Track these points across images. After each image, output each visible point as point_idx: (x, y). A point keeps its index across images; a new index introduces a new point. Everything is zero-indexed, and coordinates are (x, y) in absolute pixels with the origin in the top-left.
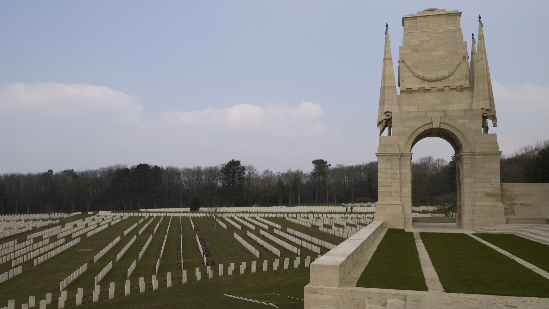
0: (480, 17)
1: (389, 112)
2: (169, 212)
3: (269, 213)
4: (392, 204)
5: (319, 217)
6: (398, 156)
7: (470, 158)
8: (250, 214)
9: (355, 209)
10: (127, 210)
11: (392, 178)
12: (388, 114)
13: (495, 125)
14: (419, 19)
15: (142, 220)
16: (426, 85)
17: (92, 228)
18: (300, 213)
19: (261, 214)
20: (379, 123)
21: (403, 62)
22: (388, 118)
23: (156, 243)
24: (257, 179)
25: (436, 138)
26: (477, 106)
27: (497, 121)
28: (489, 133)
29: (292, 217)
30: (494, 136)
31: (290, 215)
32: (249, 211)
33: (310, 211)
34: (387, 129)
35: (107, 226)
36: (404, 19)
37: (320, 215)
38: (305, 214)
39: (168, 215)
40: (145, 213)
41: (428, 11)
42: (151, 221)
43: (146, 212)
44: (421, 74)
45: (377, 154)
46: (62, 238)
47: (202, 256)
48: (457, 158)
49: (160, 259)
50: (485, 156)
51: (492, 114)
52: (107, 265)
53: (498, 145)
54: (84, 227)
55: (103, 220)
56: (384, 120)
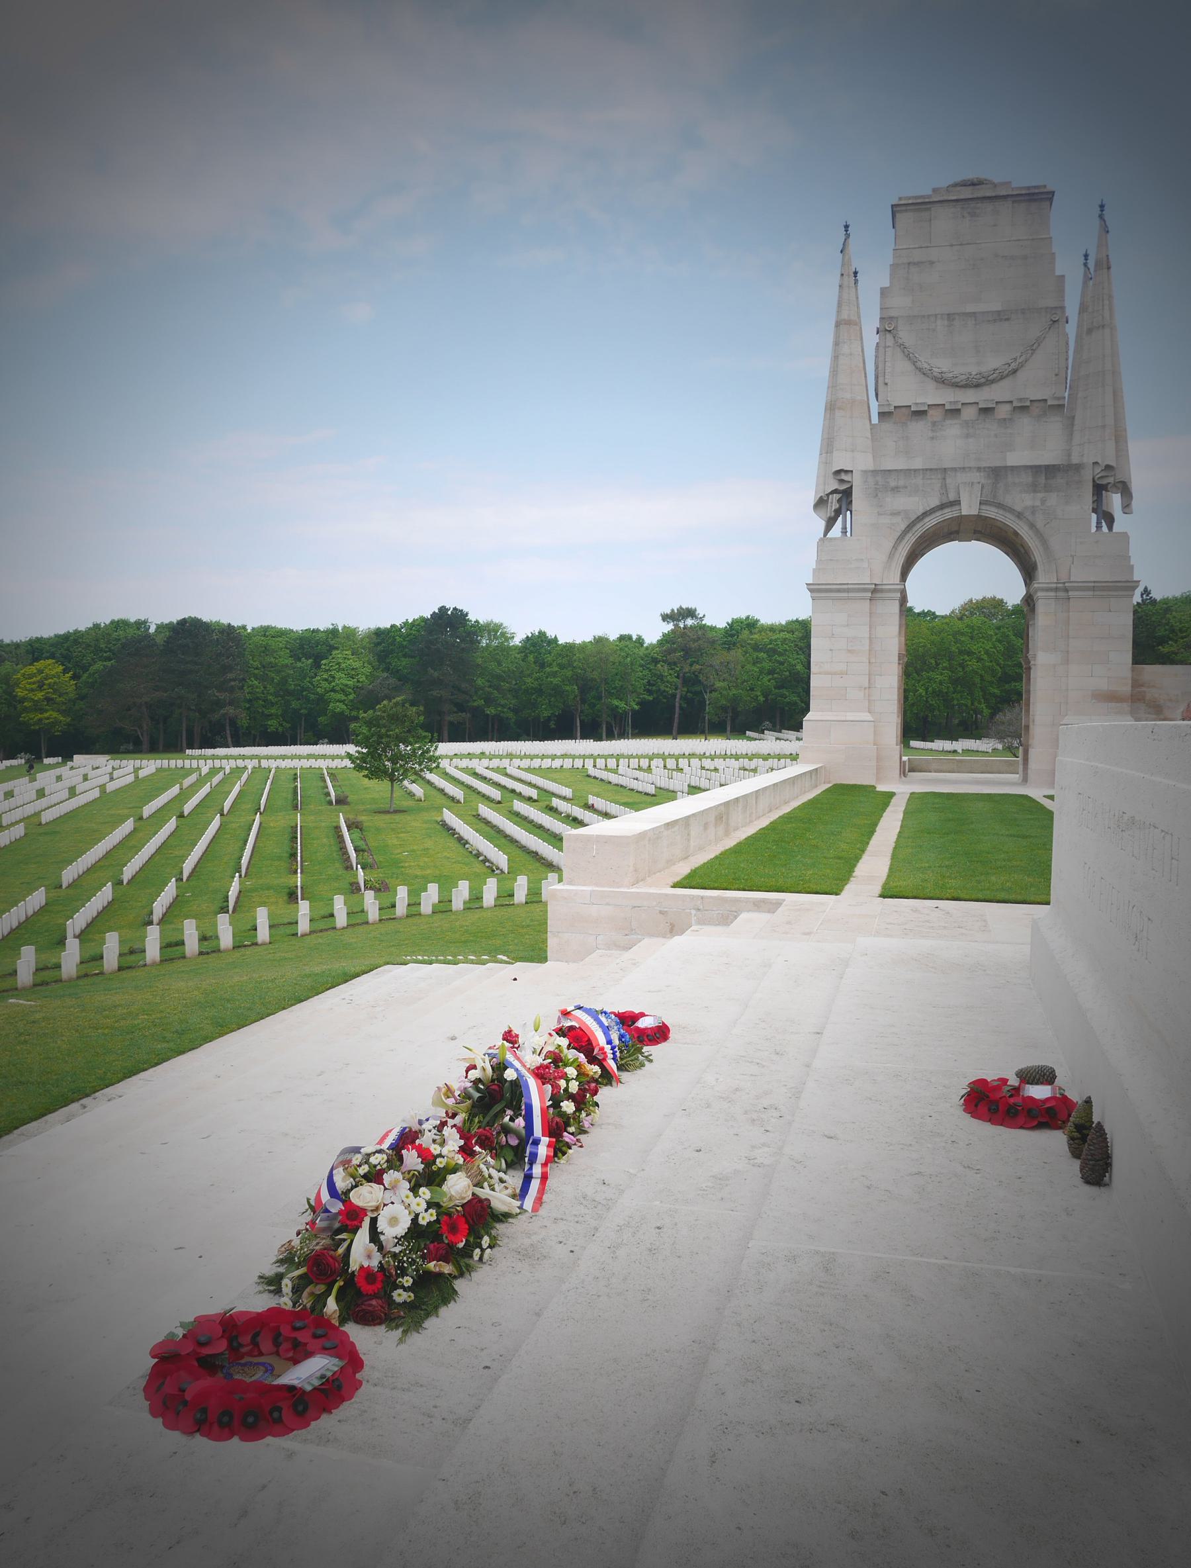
1: (846, 472)
2: (268, 758)
3: (543, 757)
4: (848, 718)
5: (680, 766)
6: (865, 590)
7: (1056, 598)
8: (490, 760)
11: (849, 651)
12: (844, 477)
13: (1126, 511)
15: (192, 778)
17: (54, 799)
18: (630, 757)
19: (532, 760)
20: (820, 503)
21: (890, 331)
22: (844, 487)
23: (231, 835)
26: (1082, 456)
27: (1132, 497)
28: (1114, 531)
29: (606, 768)
30: (1125, 536)
31: (600, 763)
32: (487, 753)
33: (656, 752)
35: (96, 794)
36: (895, 209)
37: (683, 763)
38: (642, 760)
39: (264, 763)
41: (962, 186)
42: (216, 780)
45: (812, 587)
46: (17, 823)
47: (355, 868)
49: (240, 876)
50: (1096, 593)
51: (1120, 477)
52: (165, 888)
53: (1132, 563)
54: (35, 798)
55: (85, 778)
56: (833, 492)
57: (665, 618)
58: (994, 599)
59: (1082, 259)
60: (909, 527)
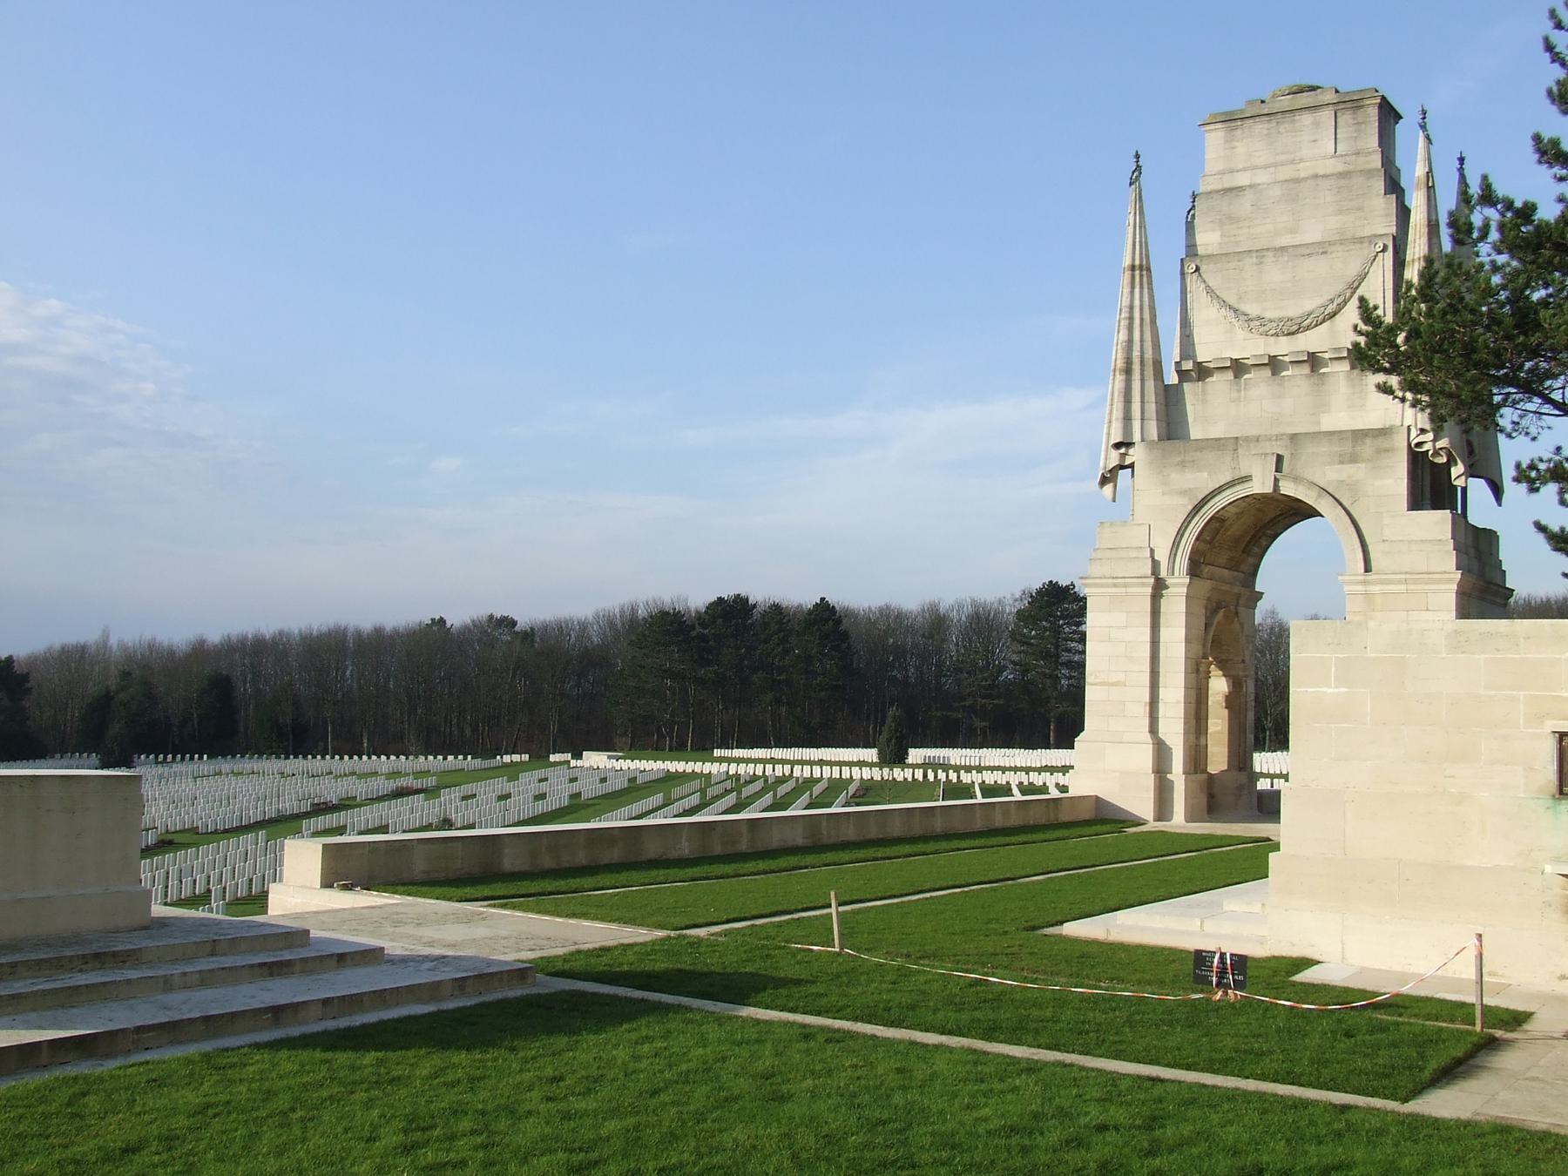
0: (1462, 160)
9: (919, 774)
10: (699, 749)
40: (808, 764)
43: (755, 759)
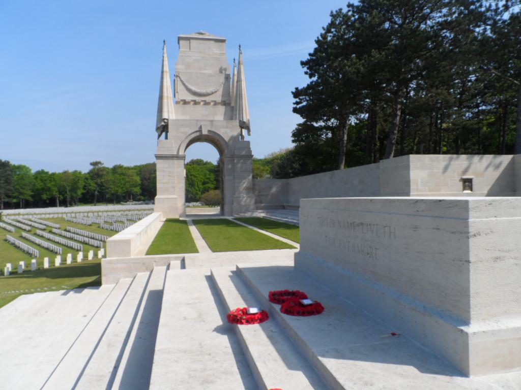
14: (192, 41)
16: (197, 99)
24: (69, 173)
25: (205, 143)
31: (69, 215)
34: (164, 134)
44: (194, 88)
48: (221, 161)
57: (91, 164)
58: (200, 159)
59: (233, 61)
60: (187, 137)
